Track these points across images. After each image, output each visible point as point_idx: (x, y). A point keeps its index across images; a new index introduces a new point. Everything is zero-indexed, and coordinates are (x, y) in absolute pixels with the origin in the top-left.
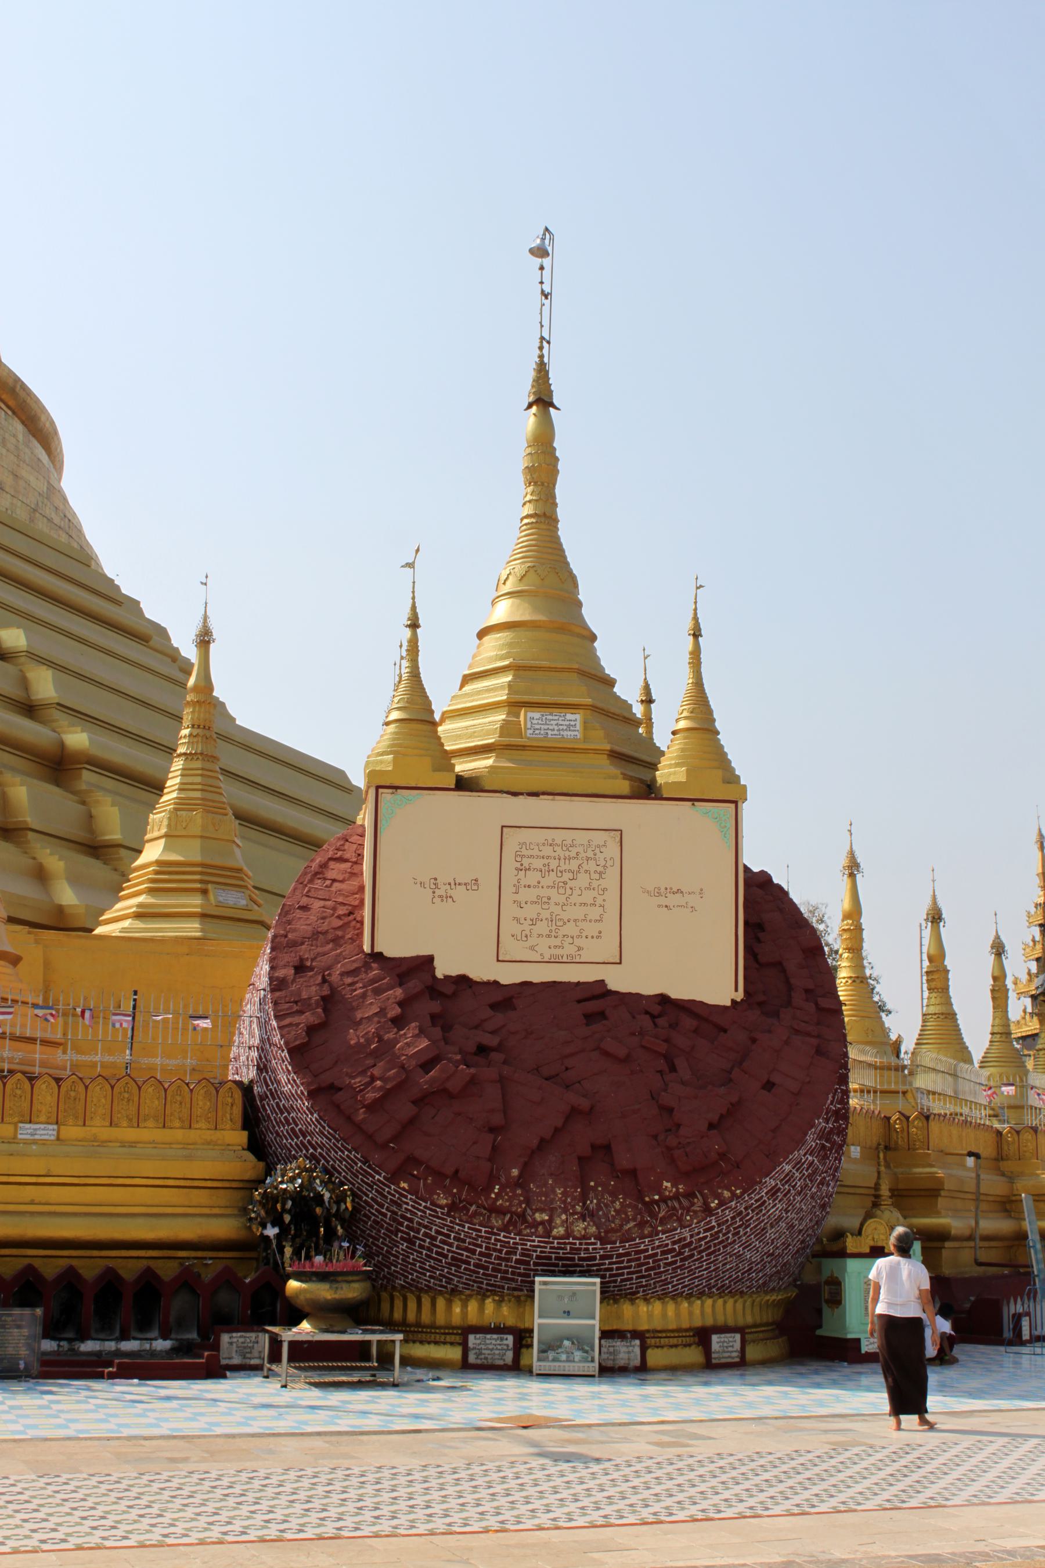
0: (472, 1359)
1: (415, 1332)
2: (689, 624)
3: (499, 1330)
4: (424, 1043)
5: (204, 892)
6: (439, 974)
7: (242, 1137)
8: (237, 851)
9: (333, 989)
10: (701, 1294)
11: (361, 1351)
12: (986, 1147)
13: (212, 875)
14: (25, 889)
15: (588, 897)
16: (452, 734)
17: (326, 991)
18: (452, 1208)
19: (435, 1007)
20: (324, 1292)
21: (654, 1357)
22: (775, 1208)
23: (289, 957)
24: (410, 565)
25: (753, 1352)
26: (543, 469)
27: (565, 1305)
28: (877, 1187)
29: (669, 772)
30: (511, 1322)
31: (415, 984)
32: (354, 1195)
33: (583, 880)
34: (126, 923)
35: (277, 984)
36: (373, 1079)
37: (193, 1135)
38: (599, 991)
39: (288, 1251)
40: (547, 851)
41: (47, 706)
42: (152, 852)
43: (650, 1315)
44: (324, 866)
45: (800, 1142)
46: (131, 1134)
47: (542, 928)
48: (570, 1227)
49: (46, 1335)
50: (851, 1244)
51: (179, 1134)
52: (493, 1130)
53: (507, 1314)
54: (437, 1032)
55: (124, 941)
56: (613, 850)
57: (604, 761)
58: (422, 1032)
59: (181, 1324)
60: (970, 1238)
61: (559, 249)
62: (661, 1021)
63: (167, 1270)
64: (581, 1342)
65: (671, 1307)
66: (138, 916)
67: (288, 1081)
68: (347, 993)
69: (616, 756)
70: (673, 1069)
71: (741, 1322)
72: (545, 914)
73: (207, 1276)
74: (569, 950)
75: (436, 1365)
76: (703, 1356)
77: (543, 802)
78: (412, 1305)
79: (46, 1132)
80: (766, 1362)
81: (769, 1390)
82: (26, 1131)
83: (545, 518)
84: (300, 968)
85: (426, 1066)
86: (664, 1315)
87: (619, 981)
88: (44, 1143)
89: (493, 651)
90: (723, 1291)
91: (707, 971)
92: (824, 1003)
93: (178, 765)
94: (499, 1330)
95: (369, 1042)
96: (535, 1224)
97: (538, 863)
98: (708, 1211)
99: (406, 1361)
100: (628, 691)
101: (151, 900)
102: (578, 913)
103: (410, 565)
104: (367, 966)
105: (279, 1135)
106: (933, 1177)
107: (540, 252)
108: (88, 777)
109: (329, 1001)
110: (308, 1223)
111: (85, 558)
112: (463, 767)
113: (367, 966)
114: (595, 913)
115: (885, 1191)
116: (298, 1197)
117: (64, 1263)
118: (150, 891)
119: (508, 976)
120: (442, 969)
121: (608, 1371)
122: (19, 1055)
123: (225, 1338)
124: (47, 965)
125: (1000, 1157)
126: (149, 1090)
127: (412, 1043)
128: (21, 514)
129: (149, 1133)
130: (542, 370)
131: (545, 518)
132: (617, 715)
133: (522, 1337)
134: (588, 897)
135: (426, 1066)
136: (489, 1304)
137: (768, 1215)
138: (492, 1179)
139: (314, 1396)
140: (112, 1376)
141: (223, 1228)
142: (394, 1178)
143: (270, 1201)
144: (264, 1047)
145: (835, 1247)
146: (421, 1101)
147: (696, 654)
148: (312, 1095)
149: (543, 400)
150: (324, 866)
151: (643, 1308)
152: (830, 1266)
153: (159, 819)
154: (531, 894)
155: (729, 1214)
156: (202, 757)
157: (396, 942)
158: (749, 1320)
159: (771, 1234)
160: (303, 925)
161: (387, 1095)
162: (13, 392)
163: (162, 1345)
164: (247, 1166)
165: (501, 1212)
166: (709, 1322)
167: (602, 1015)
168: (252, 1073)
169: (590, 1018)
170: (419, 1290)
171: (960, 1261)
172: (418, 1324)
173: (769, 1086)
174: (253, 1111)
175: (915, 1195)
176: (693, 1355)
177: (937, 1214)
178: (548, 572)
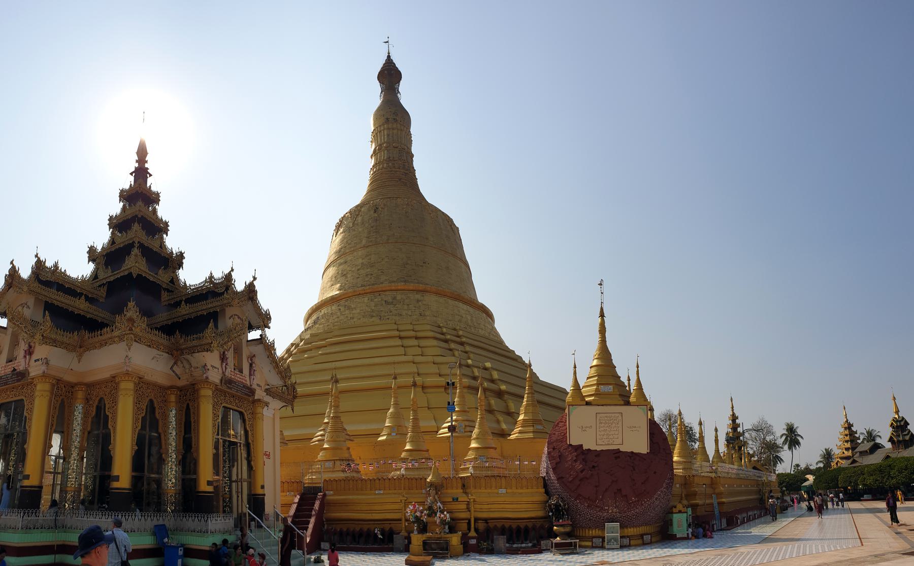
1: (582, 539)
3: (599, 537)
7: (543, 490)
11: (570, 544)
12: (708, 482)
14: (495, 425)
16: (585, 391)
20: (562, 529)
22: (657, 503)
26: (603, 330)
27: (612, 530)
29: (632, 399)
35: (549, 453)
38: (618, 451)
42: (521, 417)
46: (521, 491)
48: (613, 510)
49: (508, 542)
50: (674, 510)
55: (517, 439)
61: (604, 283)
63: (530, 525)
64: (616, 540)
69: (621, 395)
73: (538, 526)
76: (642, 542)
77: (605, 407)
79: (504, 491)
80: (657, 542)
81: (655, 550)
83: (603, 341)
84: (554, 449)
85: (582, 472)
87: (623, 449)
90: (646, 524)
91: (639, 444)
94: (599, 537)
99: (580, 546)
100: (624, 379)
107: (600, 284)
108: (506, 396)
109: (560, 456)
111: (501, 342)
119: (599, 448)
120: (585, 447)
121: (622, 547)
127: (579, 466)
128: (487, 335)
130: (602, 309)
131: (603, 341)
132: (622, 385)
133: (603, 538)
135: (582, 472)
139: (560, 557)
141: (540, 514)
144: (547, 468)
146: (581, 480)
147: (638, 371)
148: (558, 479)
149: (602, 315)
156: (532, 393)
157: (574, 442)
160: (554, 438)
163: (530, 545)
164: (543, 497)
169: (616, 458)
171: (701, 512)
175: (690, 495)
176: (640, 541)
178: (604, 353)
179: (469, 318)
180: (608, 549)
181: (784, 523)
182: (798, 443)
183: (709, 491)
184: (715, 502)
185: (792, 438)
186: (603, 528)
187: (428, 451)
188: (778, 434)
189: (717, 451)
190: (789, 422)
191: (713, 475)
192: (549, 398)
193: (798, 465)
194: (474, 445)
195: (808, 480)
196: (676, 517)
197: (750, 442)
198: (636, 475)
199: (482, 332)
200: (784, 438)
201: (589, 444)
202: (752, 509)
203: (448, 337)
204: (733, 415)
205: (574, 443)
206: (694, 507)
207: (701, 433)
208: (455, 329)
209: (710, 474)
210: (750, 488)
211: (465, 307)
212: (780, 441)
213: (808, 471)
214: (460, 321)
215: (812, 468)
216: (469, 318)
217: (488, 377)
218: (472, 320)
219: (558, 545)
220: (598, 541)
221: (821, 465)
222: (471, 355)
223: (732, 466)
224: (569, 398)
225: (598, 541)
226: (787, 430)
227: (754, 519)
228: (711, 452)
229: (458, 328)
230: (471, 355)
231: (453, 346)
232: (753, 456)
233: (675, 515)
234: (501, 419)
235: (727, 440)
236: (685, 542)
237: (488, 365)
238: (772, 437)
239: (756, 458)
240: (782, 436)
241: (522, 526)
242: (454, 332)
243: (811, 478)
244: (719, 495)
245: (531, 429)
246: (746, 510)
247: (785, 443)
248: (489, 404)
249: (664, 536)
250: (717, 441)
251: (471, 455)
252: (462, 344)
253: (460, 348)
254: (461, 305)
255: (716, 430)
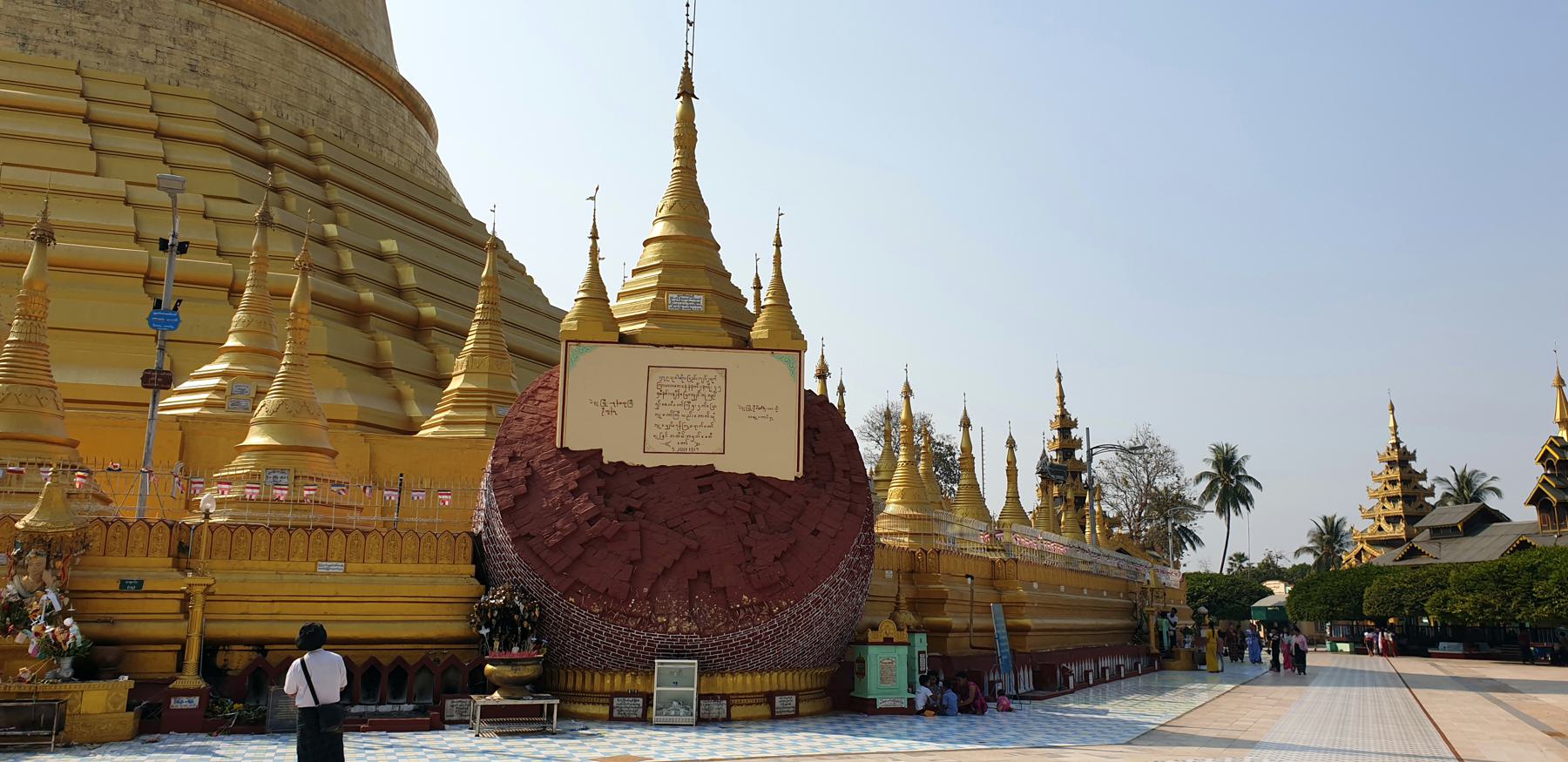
0: (615, 714)
1: (567, 695)
2: (773, 238)
3: (634, 694)
4: (592, 506)
5: (490, 408)
6: (605, 461)
7: (472, 569)
8: (514, 383)
9: (534, 472)
10: (769, 670)
12: (983, 572)
13: (492, 398)
15: (704, 411)
17: (529, 473)
18: (603, 614)
19: (601, 482)
20: (508, 672)
21: (736, 711)
23: (507, 451)
24: (593, 198)
25: (803, 708)
26: (686, 137)
27: (676, 678)
28: (897, 598)
29: (758, 332)
30: (641, 689)
31: (587, 469)
32: (541, 606)
33: (701, 400)
34: (436, 429)
35: (496, 470)
36: (556, 530)
37: (438, 568)
38: (710, 471)
39: (497, 644)
40: (678, 382)
41: (409, 289)
42: (456, 383)
43: (734, 684)
44: (535, 392)
45: (834, 570)
46: (395, 568)
47: (673, 431)
48: (679, 626)
50: (871, 636)
51: (428, 568)
52: (632, 563)
53: (639, 684)
54: (601, 499)
56: (720, 381)
57: (717, 325)
58: (590, 498)
59: (422, 693)
60: (967, 630)
62: (748, 491)
63: (412, 658)
64: (684, 702)
65: (749, 679)
66: (444, 424)
67: (501, 533)
68: (543, 474)
70: (754, 522)
71: (797, 688)
72: (676, 422)
74: (691, 445)
75: (592, 718)
76: (771, 712)
78: (579, 679)
79: (337, 567)
80: (813, 715)
81: (755, 737)
82: (323, 567)
84: (513, 458)
85: (591, 522)
86: (744, 682)
87: (723, 465)
88: (335, 574)
89: (652, 254)
90: (785, 668)
91: (778, 457)
92: (856, 479)
93: (474, 327)
94: (634, 694)
95: (555, 506)
96: (657, 624)
97: (672, 390)
98: (771, 614)
100: (742, 281)
101: (207, 412)
102: (697, 421)
103: (593, 198)
104: (557, 456)
105: (496, 568)
106: (941, 591)
108: (435, 335)
109: (528, 480)
110: (507, 626)
112: (624, 329)
113: (557, 456)
114: (707, 421)
115: (903, 601)
116: (501, 608)
117: (394, 655)
118: (453, 408)
119: (651, 462)
121: (703, 722)
122: (321, 516)
123: (448, 703)
124: (372, 456)
125: (994, 578)
126: (409, 539)
127: (583, 506)
128: (405, 167)
129: (408, 567)
133: (648, 698)
134: (704, 411)
135: (591, 522)
136: (628, 677)
137: (815, 615)
138: (630, 595)
140: (365, 730)
141: (456, 629)
142: (565, 595)
143: (482, 610)
145: (862, 638)
148: (514, 541)
149: (687, 92)
150: (535, 392)
151: (730, 679)
152: (859, 649)
153: (461, 363)
154: (667, 410)
155: (786, 617)
157: (577, 438)
158: (803, 686)
159: (816, 629)
160: (517, 430)
161: (564, 540)
162: (401, 88)
163: (411, 707)
165: (635, 616)
166: (775, 688)
167: (710, 486)
168: (481, 527)
170: (584, 669)
171: (956, 646)
172: (583, 691)
173: (816, 532)
174: (479, 553)
175: (925, 603)
176: (764, 710)
177: (944, 615)
178: (688, 204)
179: (357, 110)
180: (659, 726)
181: (1205, 697)
182: (1246, 499)
183: (983, 594)
184: (997, 621)
185: (1230, 484)
186: (648, 671)
187: (73, 444)
188: (1190, 473)
189: (1013, 497)
190: (1222, 441)
191: (996, 557)
192: (530, 335)
193: (1241, 557)
194: (256, 438)
195: (1271, 593)
196: (876, 656)
197: (1110, 490)
198: (787, 551)
199: (390, 159)
200: (1205, 483)
201: (622, 448)
202: (1111, 652)
203: (275, 152)
204: (1064, 415)
205: (574, 444)
206: (937, 634)
207: (967, 448)
208: (301, 135)
209: (992, 556)
210: (1105, 598)
211: (348, 76)
212: (1194, 492)
213: (1271, 570)
214: (322, 114)
215: (1281, 563)
216: (357, 110)
217: (384, 277)
218: (364, 119)
219: (489, 713)
220: (634, 706)
221: (1310, 559)
222: (345, 216)
223: (1053, 536)
224: (568, 324)
225: (634, 706)
226: (1216, 464)
227: (1116, 677)
228: (995, 502)
229: (311, 131)
230: (345, 216)
231: (284, 179)
232: (1117, 522)
233: (872, 650)
234: (408, 390)
235: (1042, 472)
236: (903, 721)
237: (389, 245)
238: (1171, 480)
239: (1125, 530)
240: (1199, 479)
241: (386, 661)
242: (299, 143)
243: (1280, 591)
244: (1010, 608)
245: (482, 415)
246: (1095, 654)
247: (1208, 495)
248: (377, 351)
249: (841, 699)
250: (1012, 472)
251: (241, 465)
252: (319, 179)
253: (314, 190)
254: (332, 66)
255: (1011, 444)
